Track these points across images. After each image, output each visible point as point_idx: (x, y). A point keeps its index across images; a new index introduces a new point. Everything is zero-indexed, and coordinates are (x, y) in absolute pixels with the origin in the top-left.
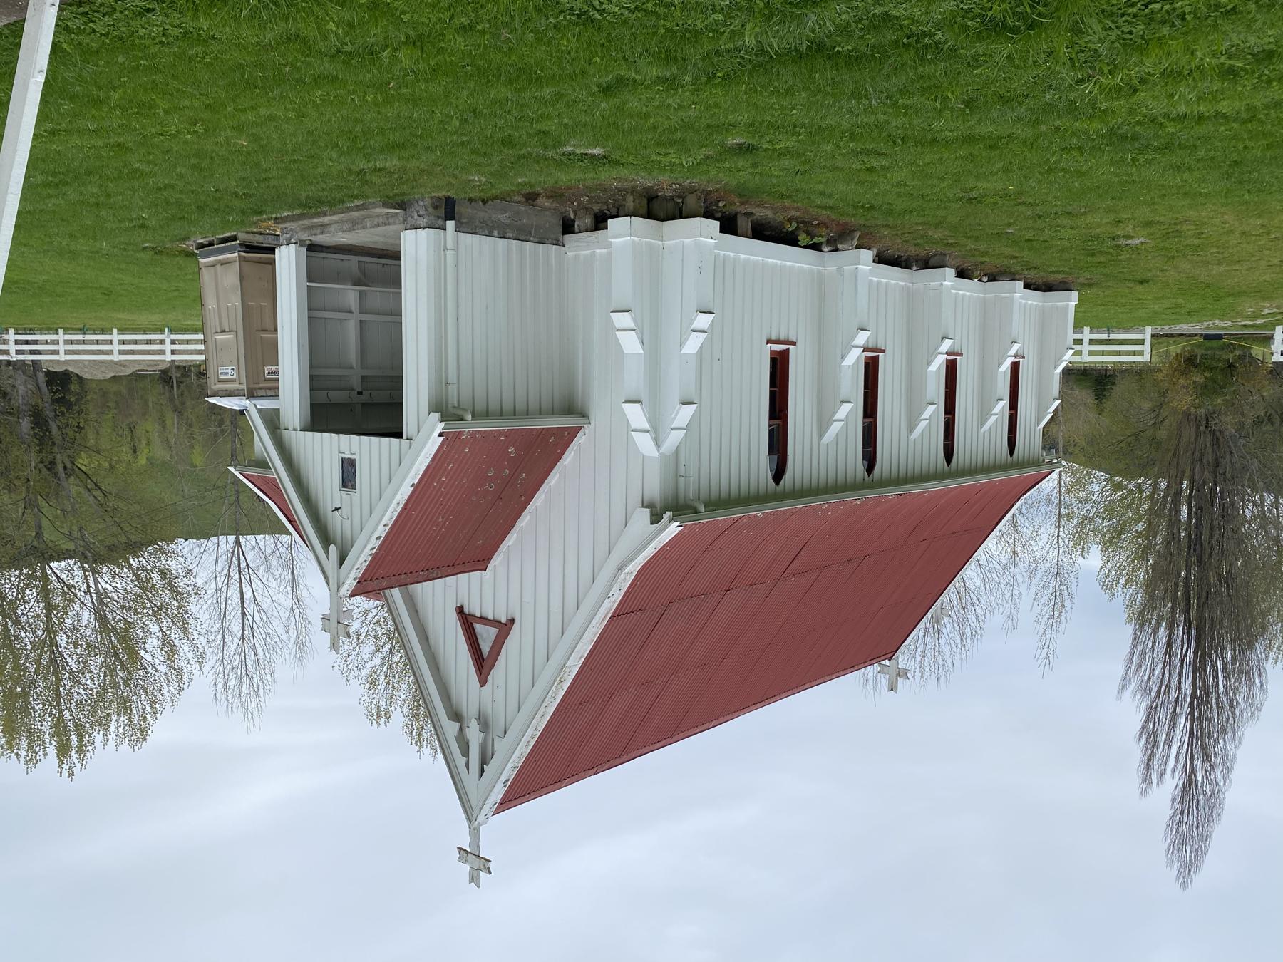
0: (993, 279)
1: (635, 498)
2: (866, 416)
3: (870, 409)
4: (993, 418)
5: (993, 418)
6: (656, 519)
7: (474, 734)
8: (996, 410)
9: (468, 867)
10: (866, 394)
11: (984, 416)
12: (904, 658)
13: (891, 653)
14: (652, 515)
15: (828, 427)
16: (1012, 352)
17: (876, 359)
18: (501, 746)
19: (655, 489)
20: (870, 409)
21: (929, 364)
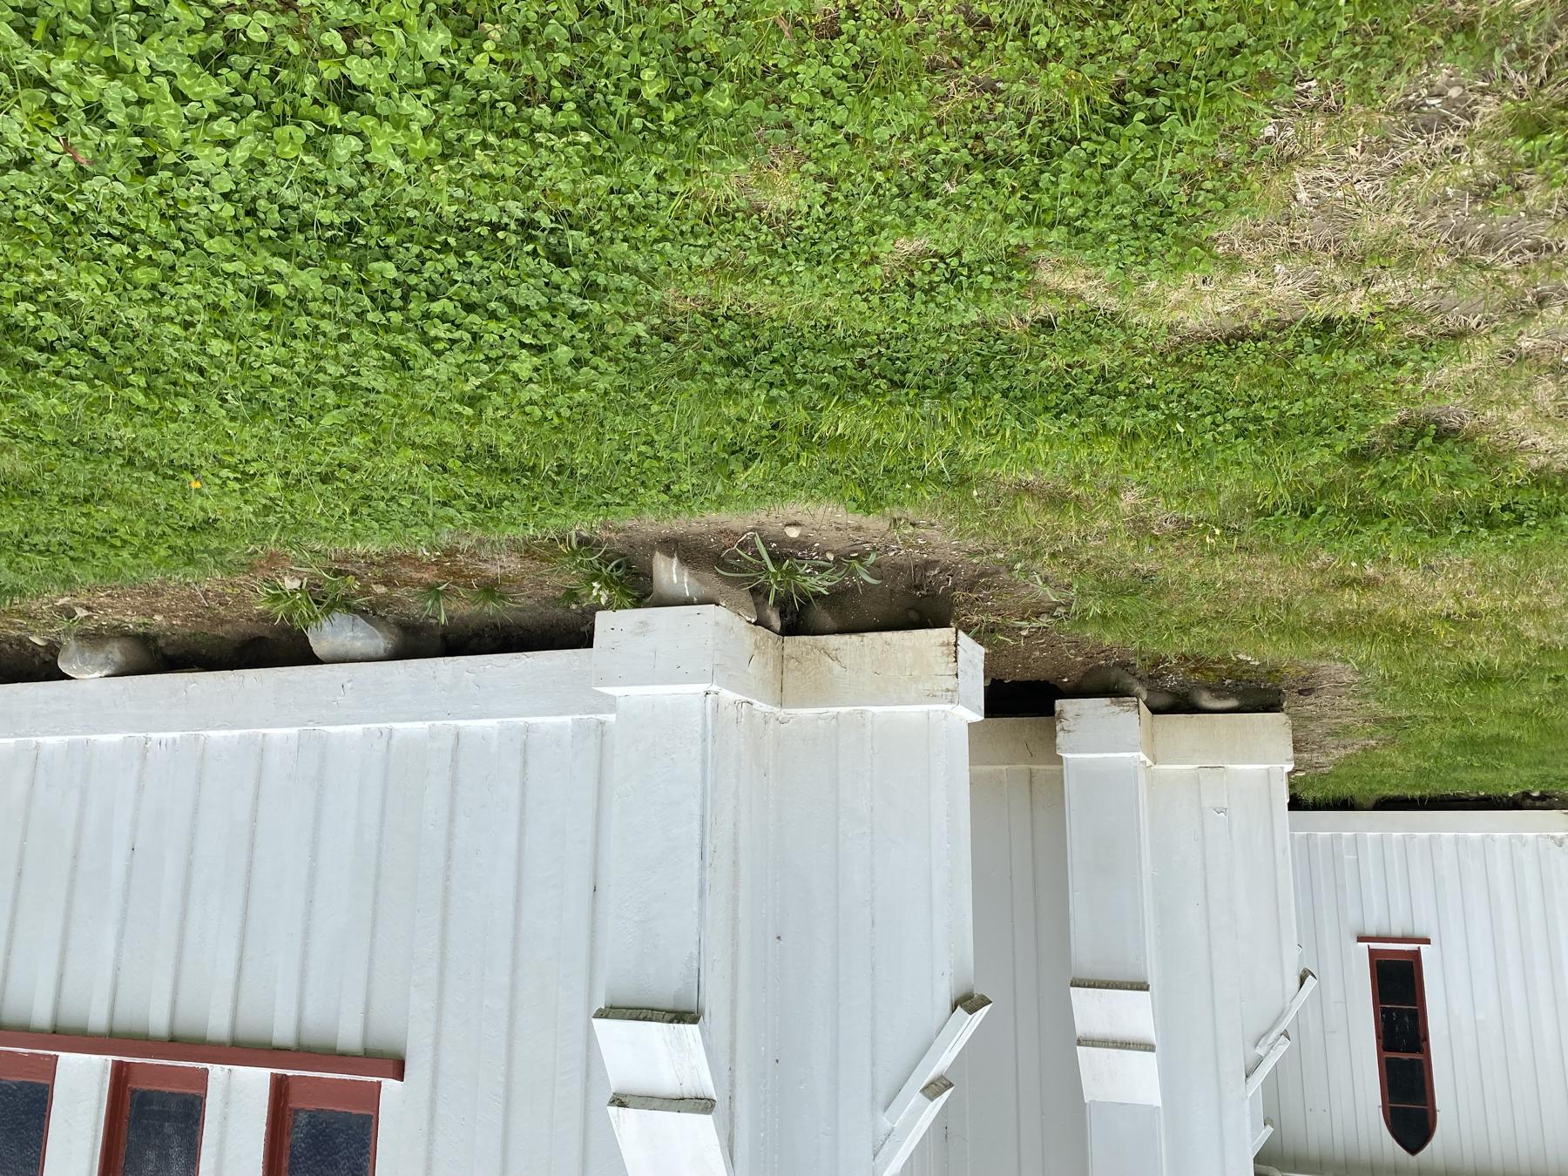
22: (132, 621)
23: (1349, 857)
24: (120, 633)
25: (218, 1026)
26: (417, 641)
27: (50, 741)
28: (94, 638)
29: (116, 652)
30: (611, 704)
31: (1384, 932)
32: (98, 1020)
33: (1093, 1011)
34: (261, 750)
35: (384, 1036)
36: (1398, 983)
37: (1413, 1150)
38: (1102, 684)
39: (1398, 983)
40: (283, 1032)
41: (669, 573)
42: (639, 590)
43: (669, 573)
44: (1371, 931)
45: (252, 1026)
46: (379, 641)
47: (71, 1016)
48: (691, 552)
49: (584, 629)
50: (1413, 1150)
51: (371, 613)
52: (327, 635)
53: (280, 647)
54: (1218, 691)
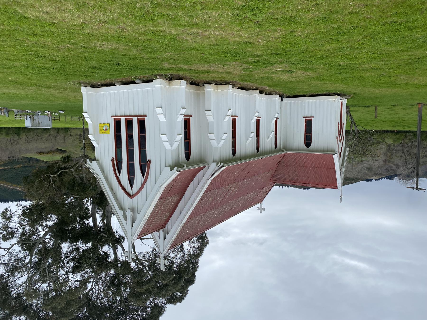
0: (270, 94)
1: (163, 164)
2: (233, 137)
3: (276, 134)
4: (271, 137)
5: (271, 137)
6: (172, 169)
7: (129, 214)
8: (271, 135)
9: (168, 305)
10: (232, 131)
11: (247, 138)
12: (265, 202)
13: (260, 201)
14: (171, 168)
15: (220, 142)
16: (276, 116)
17: (235, 119)
18: (138, 216)
19: (170, 162)
20: (276, 134)
21: (252, 120)
22: (121, 80)
23: (304, 105)
24: (120, 81)
25: (133, 114)
26: (144, 82)
27: (111, 92)
28: (118, 82)
29: (120, 83)
30: (155, 87)
31: (307, 116)
32: (123, 115)
33: (208, 113)
34: (133, 91)
35: (145, 114)
36: (309, 124)
37: (308, 148)
38: (209, 83)
39: (309, 124)
40: (138, 114)
41: (158, 77)
42: (156, 78)
43: (158, 77)
44: (305, 116)
45: (135, 114)
46: (141, 82)
47: (121, 115)
48: (159, 75)
49: (79, 103)
50: (308, 148)
51: (140, 79)
52: (137, 81)
53: (133, 82)
54: (223, 83)
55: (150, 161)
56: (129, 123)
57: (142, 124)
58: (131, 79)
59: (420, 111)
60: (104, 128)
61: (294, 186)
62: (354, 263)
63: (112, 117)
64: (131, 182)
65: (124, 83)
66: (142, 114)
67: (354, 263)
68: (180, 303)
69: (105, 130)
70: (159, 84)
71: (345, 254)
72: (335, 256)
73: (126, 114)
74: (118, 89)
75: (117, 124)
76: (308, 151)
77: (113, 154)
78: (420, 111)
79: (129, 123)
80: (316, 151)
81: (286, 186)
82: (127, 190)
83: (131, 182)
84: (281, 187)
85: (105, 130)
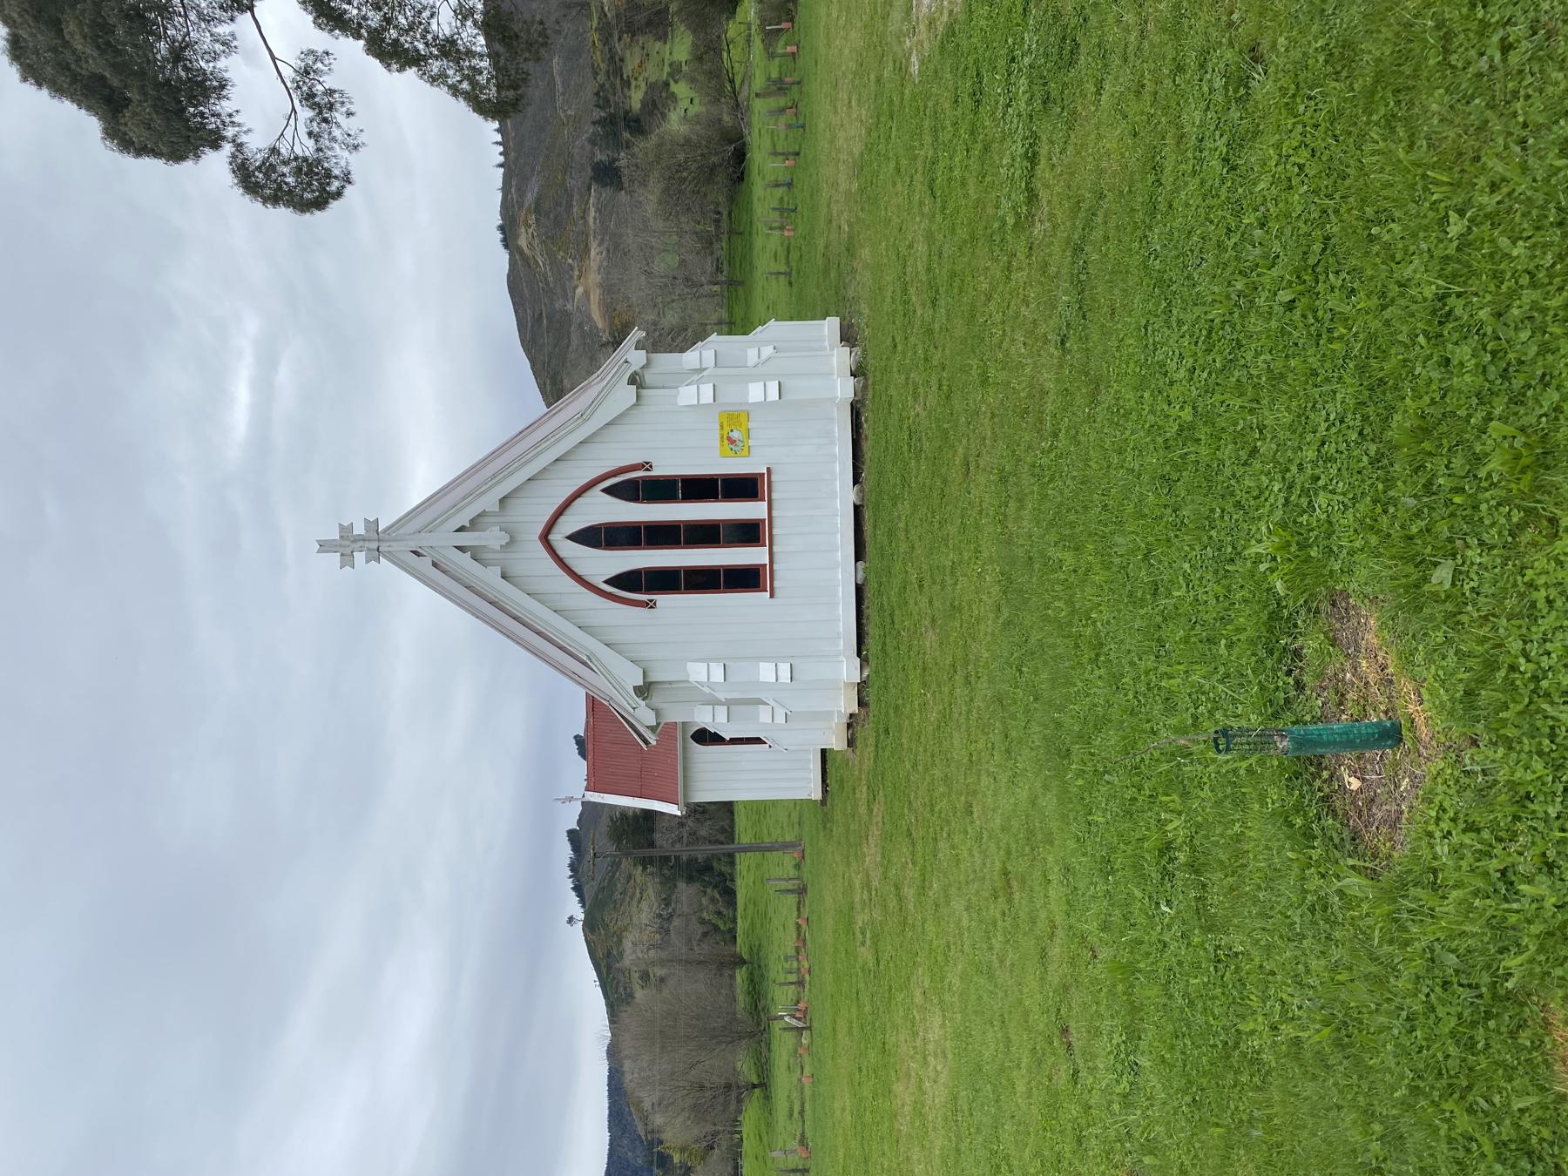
25: (775, 549)
32: (774, 513)
40: (776, 567)
53: (859, 554)
55: (649, 605)
56: (749, 533)
57: (747, 579)
58: (870, 549)
59: (785, 846)
60: (735, 435)
61: (506, 189)
62: (243, 392)
63: (769, 470)
64: (592, 537)
65: (858, 510)
66: (776, 584)
67: (243, 392)
68: (25, 80)
69: (729, 439)
70: (848, 670)
71: (268, 361)
72: (251, 326)
73: (776, 523)
74: (844, 496)
75: (745, 487)
76: (684, 739)
77: (665, 467)
78: (785, 846)
79: (749, 533)
80: (685, 759)
81: (501, 159)
82: (562, 519)
83: (592, 537)
84: (499, 138)
85: (729, 439)
